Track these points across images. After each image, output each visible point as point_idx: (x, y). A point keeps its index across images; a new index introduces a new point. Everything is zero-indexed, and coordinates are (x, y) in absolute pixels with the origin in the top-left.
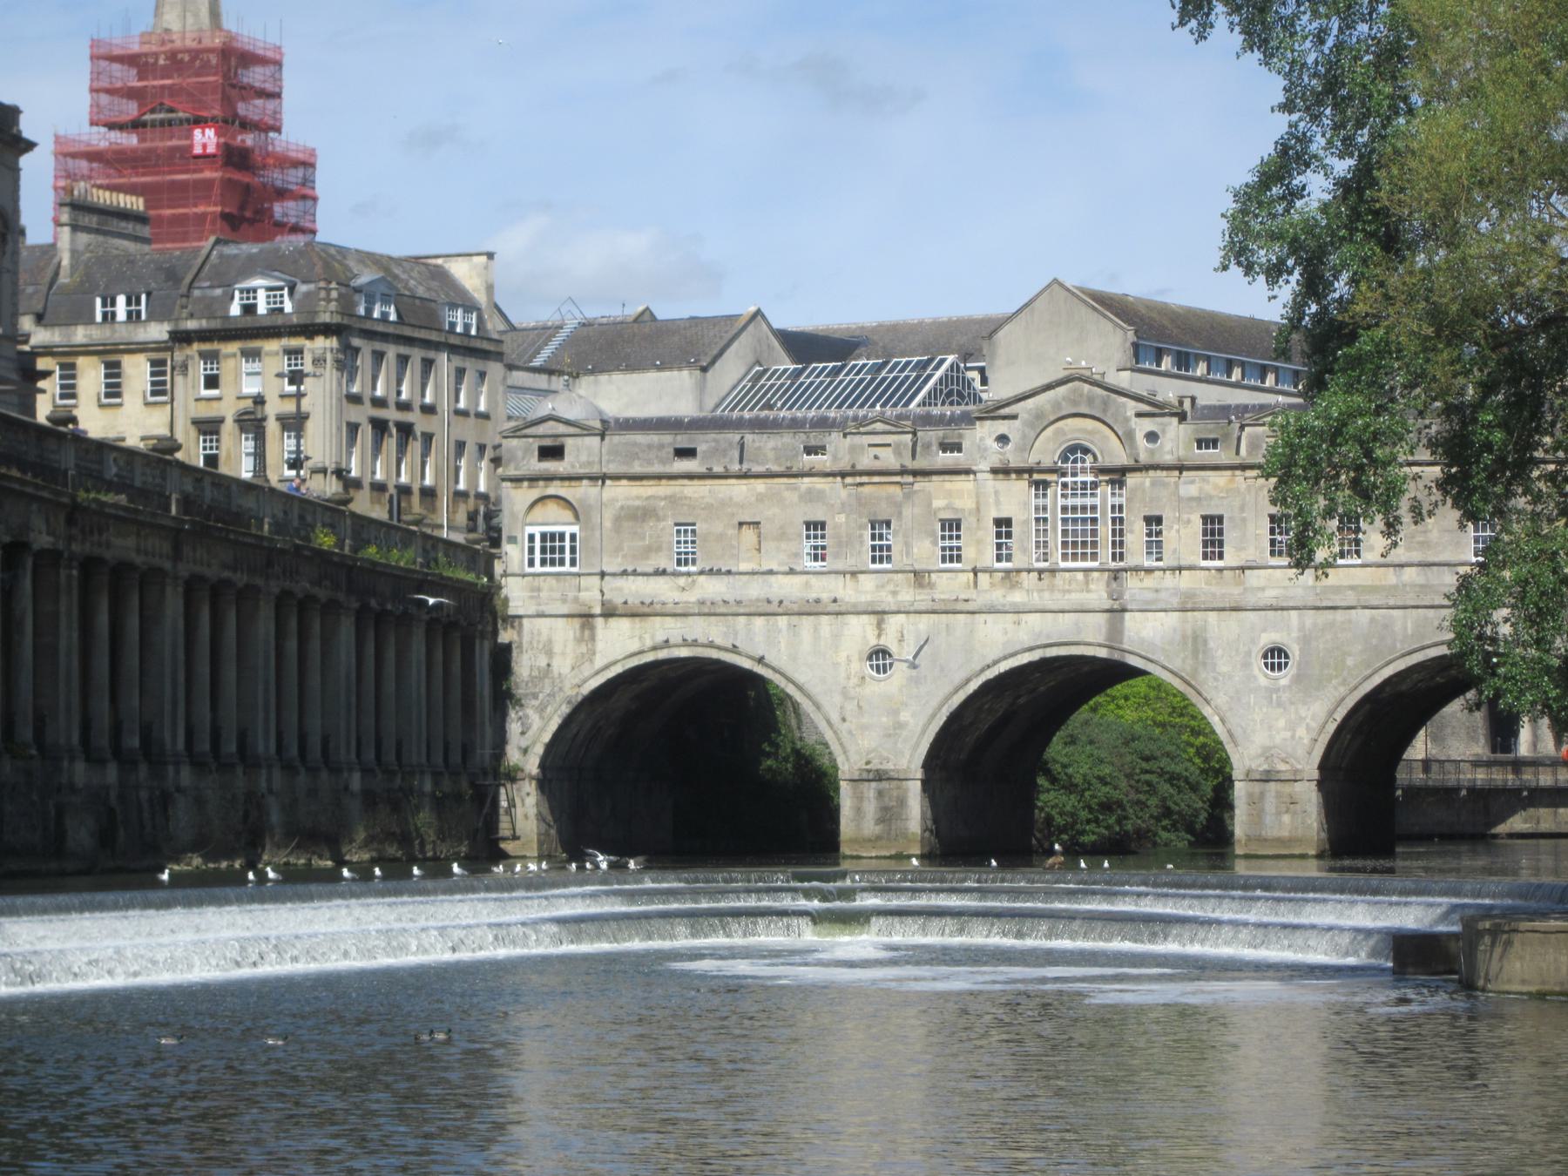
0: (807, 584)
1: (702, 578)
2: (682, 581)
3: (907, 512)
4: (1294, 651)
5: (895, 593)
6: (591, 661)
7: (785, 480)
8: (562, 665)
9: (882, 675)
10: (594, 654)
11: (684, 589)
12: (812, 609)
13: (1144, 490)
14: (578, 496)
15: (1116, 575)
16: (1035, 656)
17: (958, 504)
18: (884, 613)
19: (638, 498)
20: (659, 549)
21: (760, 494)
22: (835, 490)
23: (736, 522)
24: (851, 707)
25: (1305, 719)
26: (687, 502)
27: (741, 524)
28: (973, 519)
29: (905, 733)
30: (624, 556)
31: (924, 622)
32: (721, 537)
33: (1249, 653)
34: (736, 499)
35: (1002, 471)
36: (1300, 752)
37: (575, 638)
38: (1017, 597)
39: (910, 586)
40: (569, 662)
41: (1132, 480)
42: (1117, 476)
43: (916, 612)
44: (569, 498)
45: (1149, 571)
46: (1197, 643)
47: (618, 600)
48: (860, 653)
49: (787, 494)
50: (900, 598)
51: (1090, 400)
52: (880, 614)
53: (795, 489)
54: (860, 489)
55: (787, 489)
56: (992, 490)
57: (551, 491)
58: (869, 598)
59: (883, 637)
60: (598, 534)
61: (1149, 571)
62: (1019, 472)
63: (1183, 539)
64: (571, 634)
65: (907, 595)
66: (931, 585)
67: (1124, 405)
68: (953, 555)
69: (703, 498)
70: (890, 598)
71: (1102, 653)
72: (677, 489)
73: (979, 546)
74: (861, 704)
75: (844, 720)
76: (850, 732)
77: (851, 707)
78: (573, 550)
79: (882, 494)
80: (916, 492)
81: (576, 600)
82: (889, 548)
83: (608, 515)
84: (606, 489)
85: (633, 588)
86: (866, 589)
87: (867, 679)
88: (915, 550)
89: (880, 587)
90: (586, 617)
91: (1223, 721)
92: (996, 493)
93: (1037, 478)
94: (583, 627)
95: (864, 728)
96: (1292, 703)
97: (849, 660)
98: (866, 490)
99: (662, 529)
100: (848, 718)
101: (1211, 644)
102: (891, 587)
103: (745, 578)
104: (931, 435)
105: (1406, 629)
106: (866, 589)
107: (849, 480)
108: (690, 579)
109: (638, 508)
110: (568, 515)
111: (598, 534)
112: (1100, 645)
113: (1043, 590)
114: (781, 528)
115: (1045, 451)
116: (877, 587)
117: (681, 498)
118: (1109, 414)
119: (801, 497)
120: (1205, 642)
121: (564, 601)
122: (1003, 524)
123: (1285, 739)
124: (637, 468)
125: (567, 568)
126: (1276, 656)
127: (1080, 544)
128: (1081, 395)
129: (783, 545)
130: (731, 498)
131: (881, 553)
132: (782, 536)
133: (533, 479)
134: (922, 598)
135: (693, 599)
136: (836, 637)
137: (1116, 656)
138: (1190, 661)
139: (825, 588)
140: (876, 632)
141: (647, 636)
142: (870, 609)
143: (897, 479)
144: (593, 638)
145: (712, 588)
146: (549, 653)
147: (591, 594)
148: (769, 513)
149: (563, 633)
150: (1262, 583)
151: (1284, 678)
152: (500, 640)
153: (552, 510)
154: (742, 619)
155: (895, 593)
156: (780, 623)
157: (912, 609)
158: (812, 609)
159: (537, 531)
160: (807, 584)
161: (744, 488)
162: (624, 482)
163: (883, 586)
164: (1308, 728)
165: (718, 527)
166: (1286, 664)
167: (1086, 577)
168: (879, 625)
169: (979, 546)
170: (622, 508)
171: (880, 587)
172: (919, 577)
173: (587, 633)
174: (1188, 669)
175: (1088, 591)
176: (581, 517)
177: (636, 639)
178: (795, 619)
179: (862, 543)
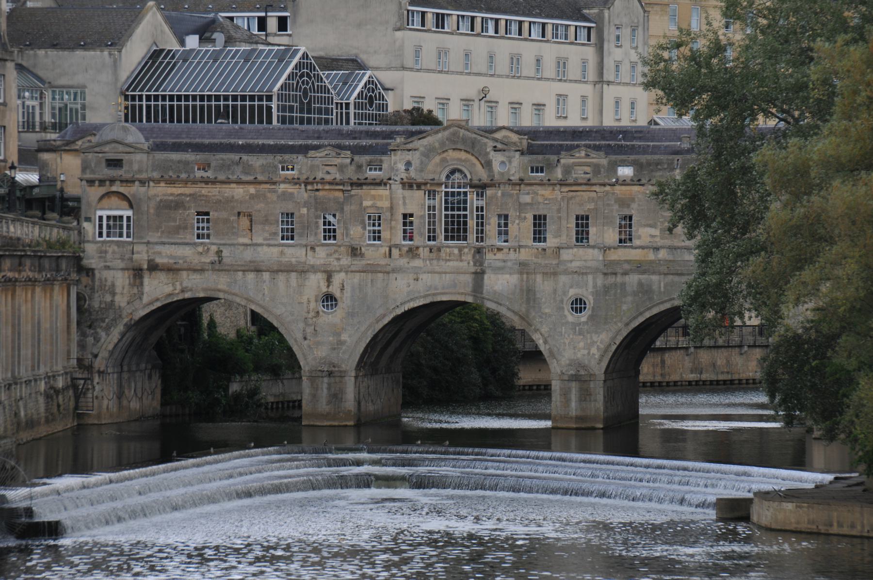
0: (282, 253)
2: (200, 249)
3: (347, 208)
4: (590, 300)
5: (338, 259)
6: (141, 299)
7: (268, 186)
8: (121, 301)
10: (143, 294)
11: (201, 253)
12: (288, 269)
13: (497, 198)
14: (132, 192)
15: (479, 251)
16: (428, 301)
17: (379, 204)
18: (334, 271)
19: (172, 195)
20: (185, 228)
21: (252, 194)
22: (301, 194)
23: (236, 212)
24: (309, 330)
25: (596, 342)
26: (204, 198)
28: (388, 214)
29: (344, 348)
30: (163, 232)
31: (357, 278)
32: (226, 221)
33: (562, 301)
34: (236, 197)
35: (409, 185)
36: (593, 363)
37: (130, 284)
39: (348, 255)
40: (126, 299)
41: (489, 192)
42: (481, 188)
43: (352, 272)
44: (126, 194)
45: (500, 249)
46: (529, 294)
47: (159, 260)
48: (317, 296)
49: (269, 195)
50: (341, 263)
53: (274, 192)
54: (317, 193)
55: (269, 192)
56: (401, 196)
57: (114, 188)
58: (322, 262)
59: (331, 287)
60: (145, 217)
61: (500, 249)
64: (127, 282)
65: (346, 261)
66: (362, 255)
67: (485, 144)
69: (215, 196)
70: (335, 263)
72: (198, 189)
73: (394, 233)
74: (316, 329)
75: (305, 339)
76: (309, 346)
77: (309, 330)
78: (128, 227)
80: (352, 196)
81: (131, 259)
82: (334, 230)
83: (152, 204)
84: (151, 188)
85: (168, 252)
86: (320, 256)
87: (321, 313)
88: (352, 232)
89: (329, 255)
90: (137, 273)
91: (545, 342)
92: (404, 198)
93: (428, 187)
94: (135, 276)
95: (318, 344)
96: (588, 333)
97: (309, 301)
98: (321, 193)
99: (188, 215)
100: (309, 338)
101: (538, 296)
102: (336, 256)
104: (364, 159)
105: (660, 287)
106: (320, 256)
107: (309, 187)
109: (172, 201)
110: (125, 204)
111: (145, 217)
113: (433, 259)
114: (266, 216)
116: (327, 255)
117: (200, 196)
118: (476, 150)
119: (278, 197)
120: (535, 294)
121: (122, 259)
123: (584, 355)
125: (124, 239)
126: (578, 305)
127: (313, 249)
128: (458, 137)
129: (267, 228)
130: (233, 197)
131: (330, 233)
132: (266, 221)
133: (102, 182)
134: (359, 263)
135: (208, 261)
136: (301, 286)
138: (524, 305)
139: (294, 254)
140: (326, 284)
141: (178, 283)
143: (341, 187)
144: (142, 284)
146: (114, 294)
147: (142, 256)
149: (121, 280)
150: (570, 257)
151: (584, 317)
152: (758, 375)
153: (114, 200)
154: (240, 273)
155: (338, 259)
156: (264, 277)
157: (350, 269)
158: (288, 269)
159: (105, 213)
160: (282, 253)
161: (241, 190)
163: (331, 255)
164: (598, 348)
165: (224, 215)
166: (585, 308)
167: (460, 251)
170: (161, 201)
172: (355, 252)
173: (138, 281)
174: (524, 310)
176: (134, 206)
177: (171, 285)
179: (317, 227)
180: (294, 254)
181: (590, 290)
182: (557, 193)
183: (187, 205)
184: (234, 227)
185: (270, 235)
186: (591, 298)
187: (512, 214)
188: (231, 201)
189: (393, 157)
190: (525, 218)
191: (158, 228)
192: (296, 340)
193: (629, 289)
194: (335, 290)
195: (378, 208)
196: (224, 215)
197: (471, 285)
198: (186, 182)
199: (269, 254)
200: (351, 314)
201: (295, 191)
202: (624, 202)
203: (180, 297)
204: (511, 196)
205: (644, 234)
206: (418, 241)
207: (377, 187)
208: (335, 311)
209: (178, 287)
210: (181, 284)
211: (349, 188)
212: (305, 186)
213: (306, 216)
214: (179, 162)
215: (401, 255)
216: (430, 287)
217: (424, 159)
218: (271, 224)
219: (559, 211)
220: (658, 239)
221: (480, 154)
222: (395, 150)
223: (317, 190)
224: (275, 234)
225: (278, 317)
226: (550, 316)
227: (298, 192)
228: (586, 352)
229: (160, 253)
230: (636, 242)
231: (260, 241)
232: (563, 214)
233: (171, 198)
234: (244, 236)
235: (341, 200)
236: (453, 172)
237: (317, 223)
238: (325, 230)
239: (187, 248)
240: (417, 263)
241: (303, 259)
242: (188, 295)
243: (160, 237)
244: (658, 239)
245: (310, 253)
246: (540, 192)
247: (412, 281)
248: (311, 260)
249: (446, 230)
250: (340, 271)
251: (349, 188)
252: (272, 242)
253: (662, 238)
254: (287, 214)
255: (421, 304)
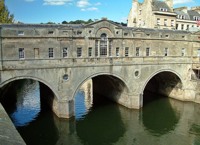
1: (26, 61)
3: (71, 46)
5: (69, 63)
7: (44, 39)
9: (66, 80)
17: (81, 44)
18: (68, 67)
20: (15, 54)
22: (57, 42)
24: (60, 87)
27: (34, 48)
29: (71, 92)
32: (30, 52)
35: (91, 38)
38: (93, 64)
41: (114, 41)
42: (111, 40)
46: (125, 72)
48: (62, 76)
51: (107, 24)
52: (66, 68)
61: (117, 58)
62: (94, 38)
63: (122, 52)
65: (71, 63)
66: (76, 61)
68: (79, 55)
71: (109, 74)
74: (63, 86)
75: (59, 90)
79: (139, 44)
82: (67, 53)
86: (63, 63)
89: (66, 62)
92: (89, 42)
93: (96, 39)
95: (63, 91)
99: (16, 50)
100: (60, 89)
102: (68, 62)
103: (36, 60)
106: (63, 63)
107: (58, 39)
108: (23, 61)
112: (109, 72)
115: (98, 36)
117: (20, 43)
119: (48, 42)
122: (90, 48)
124: (9, 36)
128: (105, 24)
130: (32, 43)
132: (44, 51)
136: (57, 72)
137: (111, 74)
142: (64, 67)
143: (69, 39)
145: (28, 63)
148: (41, 46)
151: (139, 74)
154: (36, 70)
155: (69, 63)
162: (6, 39)
163: (67, 62)
165: (29, 49)
166: (68, 78)
168: (66, 71)
169: (84, 54)
171: (66, 62)
172: (74, 60)
174: (123, 76)
175: (106, 62)
178: (48, 70)
180: (55, 62)
181: (140, 69)
182: (132, 41)
183: (16, 46)
184: (33, 54)
185: (46, 56)
186: (140, 71)
187: (120, 47)
188: (32, 44)
189: (85, 29)
190: (123, 49)
191: (5, 55)
192: (56, 91)
193: (149, 68)
194: (68, 73)
195: (81, 46)
196: (29, 49)
197: (109, 69)
198: (15, 38)
199: (47, 62)
200: (73, 81)
201: (53, 40)
202: (148, 45)
203: (15, 79)
204: (120, 42)
205: (152, 53)
206: (93, 56)
207: (80, 39)
208: (68, 80)
209: (14, 76)
210: (15, 75)
211: (72, 39)
212: (57, 39)
213: (58, 49)
214: (12, 31)
215: (88, 61)
216: (97, 71)
217: (95, 30)
218: (46, 52)
219: (132, 47)
220: (155, 55)
221: (111, 29)
222: (86, 27)
223: (61, 40)
224: (47, 55)
225: (49, 84)
226: (130, 77)
227: (55, 41)
228: (139, 87)
229: (6, 64)
230: (149, 56)
231: (43, 58)
232: (133, 47)
233: (9, 44)
234: (36, 57)
235: (69, 43)
236: (102, 35)
237: (61, 51)
238: (63, 54)
239: (16, 62)
240: (93, 64)
241: (57, 63)
242: (18, 78)
243: (6, 58)
244: (155, 55)
245: (59, 61)
246: (127, 41)
247: (92, 69)
248: (59, 63)
249: (106, 50)
250: (69, 67)
251: (72, 39)
252: (46, 58)
253: (156, 54)
254: (51, 49)
255: (102, 74)
